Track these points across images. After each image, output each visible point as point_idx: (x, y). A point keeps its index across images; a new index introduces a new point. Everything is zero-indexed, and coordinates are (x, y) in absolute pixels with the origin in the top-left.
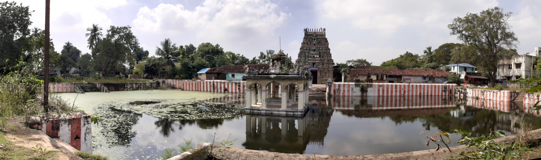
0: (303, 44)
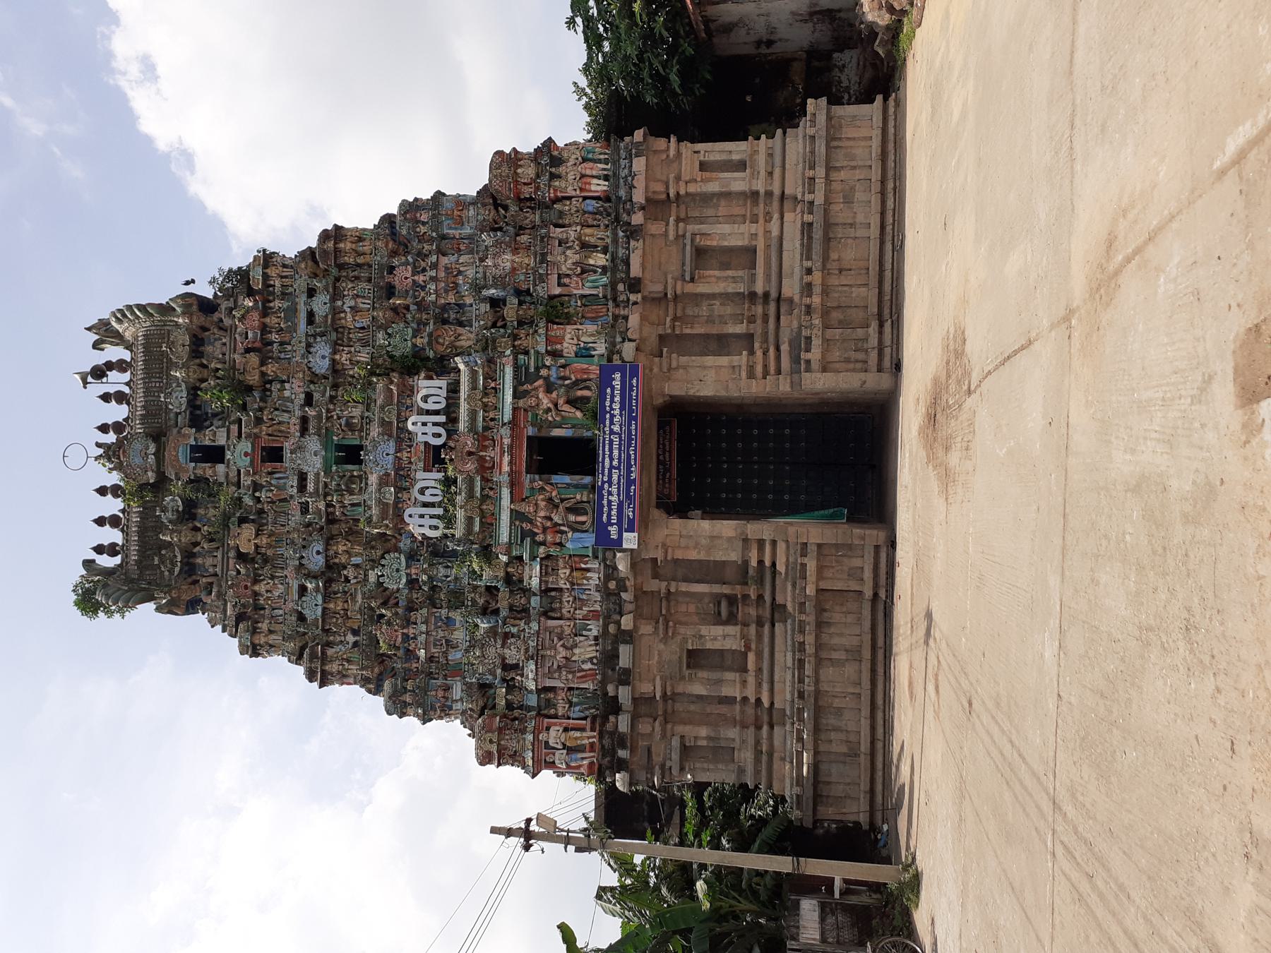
0: (252, 630)
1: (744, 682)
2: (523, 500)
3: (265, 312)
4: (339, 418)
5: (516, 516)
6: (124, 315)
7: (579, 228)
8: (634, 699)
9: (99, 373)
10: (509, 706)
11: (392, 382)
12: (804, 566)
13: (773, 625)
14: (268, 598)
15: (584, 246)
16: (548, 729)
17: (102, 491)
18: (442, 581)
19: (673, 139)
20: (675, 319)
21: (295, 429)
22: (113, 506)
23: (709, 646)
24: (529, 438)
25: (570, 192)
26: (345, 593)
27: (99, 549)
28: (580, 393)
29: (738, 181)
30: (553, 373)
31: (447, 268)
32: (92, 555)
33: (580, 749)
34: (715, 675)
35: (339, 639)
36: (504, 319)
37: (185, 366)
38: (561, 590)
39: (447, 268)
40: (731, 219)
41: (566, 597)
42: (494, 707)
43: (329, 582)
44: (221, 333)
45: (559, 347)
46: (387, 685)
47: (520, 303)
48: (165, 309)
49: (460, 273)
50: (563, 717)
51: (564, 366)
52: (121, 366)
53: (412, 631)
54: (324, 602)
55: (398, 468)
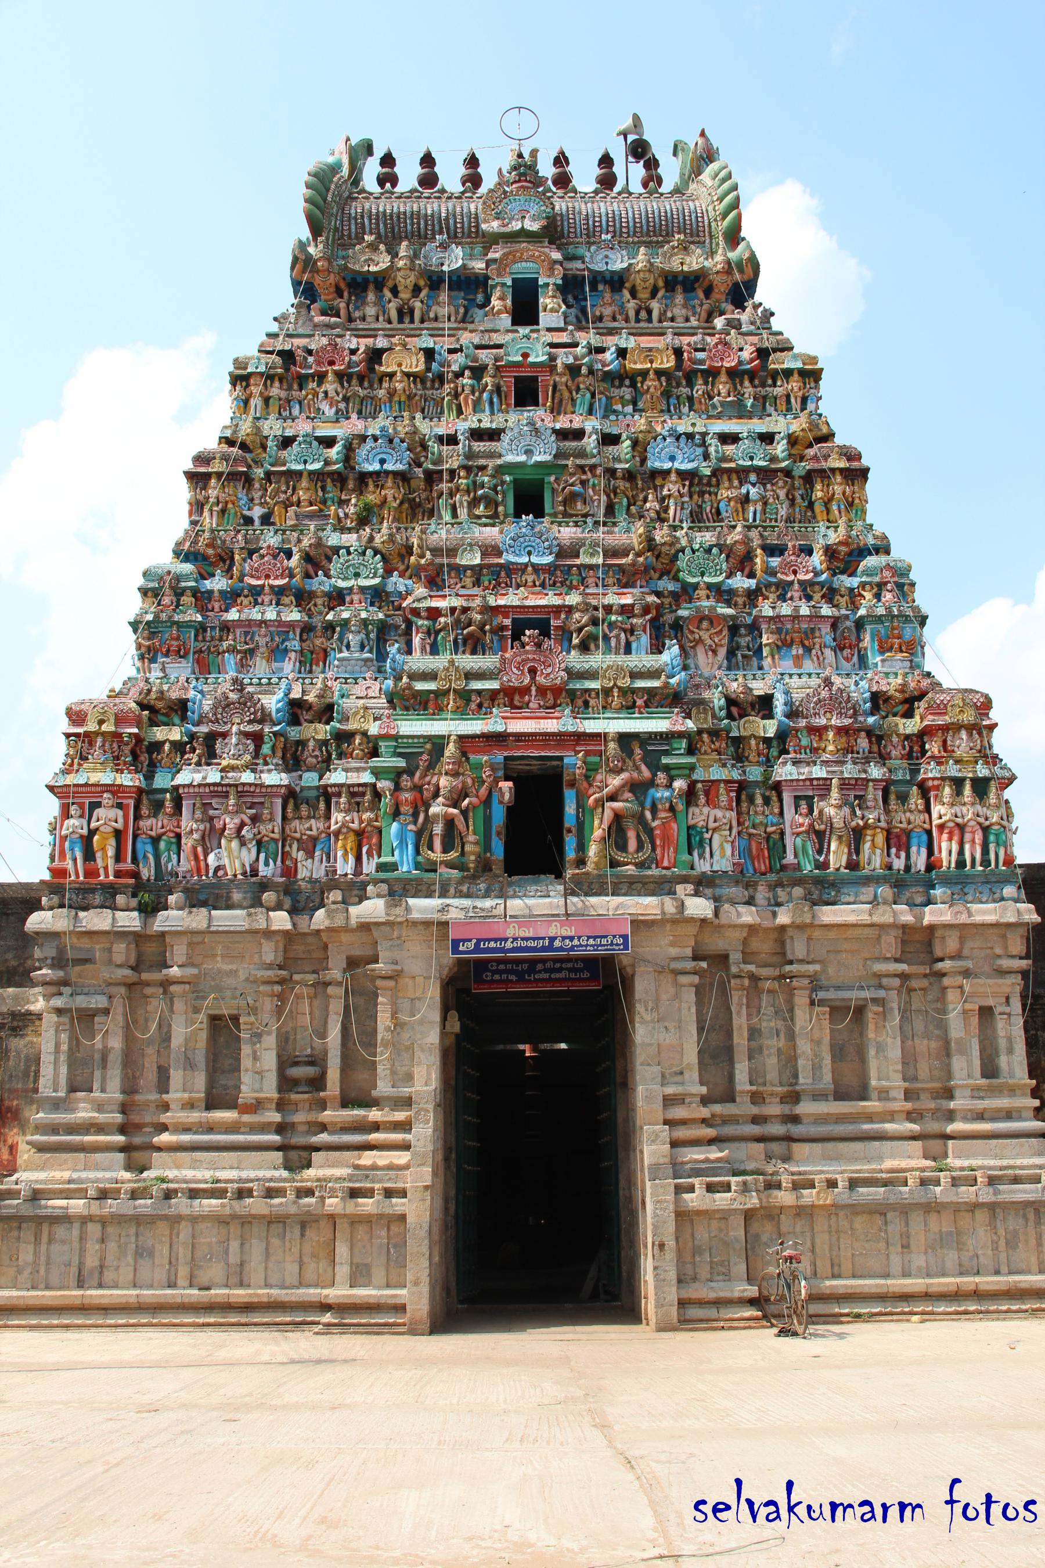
1: (190, 1105)
2: (464, 754)
3: (734, 374)
4: (583, 483)
5: (437, 744)
6: (724, 181)
7: (883, 824)
8: (163, 934)
9: (639, 150)
10: (156, 746)
11: (638, 555)
12: (369, 1193)
13: (278, 1149)
14: (316, 394)
15: (857, 835)
16: (120, 806)
17: (472, 162)
18: (341, 639)
19: (1024, 964)
20: (754, 978)
21: (563, 423)
22: (450, 175)
23: (246, 1050)
24: (561, 759)
25: (936, 809)
26: (324, 502)
27: (388, 160)
28: (631, 835)
29: (965, 1069)
30: (662, 794)
31: (813, 630)
32: (379, 153)
33: (89, 855)
34: (200, 1057)
35: (257, 495)
36: (741, 716)
37: (651, 268)
38: (328, 817)
39: (813, 630)
40: (909, 1059)
41: (316, 826)
42: (153, 723)
43: (340, 479)
44: (704, 315)
45: (702, 800)
46: (188, 567)
47: (767, 741)
48: (734, 237)
49: (808, 650)
50: (136, 828)
51: (672, 809)
52: (652, 179)
53: (267, 599)
54: (311, 473)
55: (511, 569)
